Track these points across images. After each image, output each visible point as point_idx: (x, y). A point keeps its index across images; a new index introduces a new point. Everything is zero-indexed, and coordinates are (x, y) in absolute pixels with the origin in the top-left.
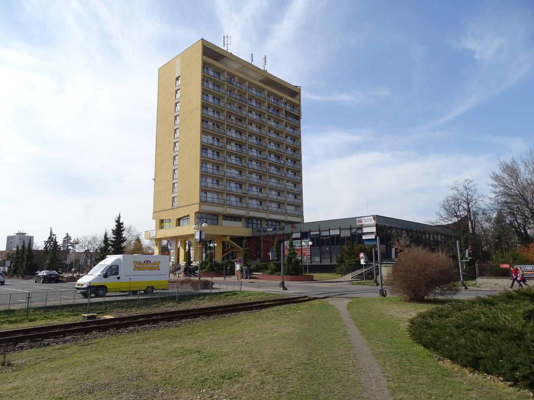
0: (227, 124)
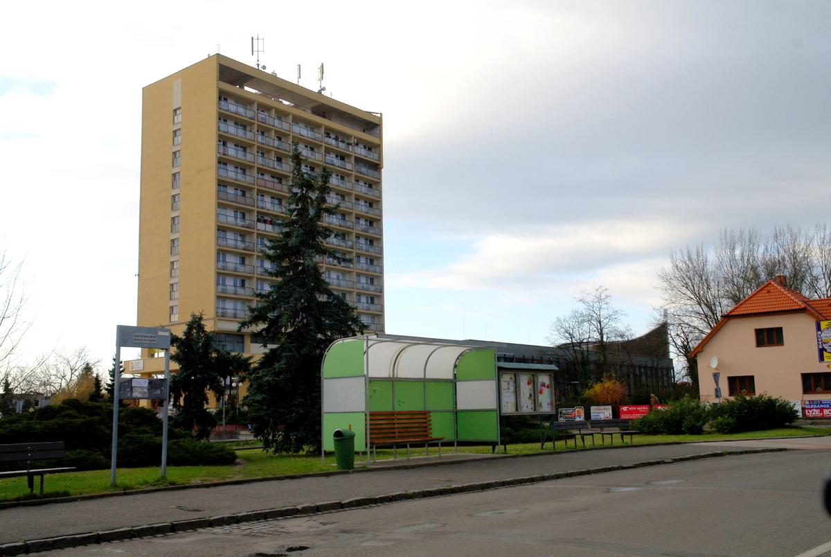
0: (258, 146)
